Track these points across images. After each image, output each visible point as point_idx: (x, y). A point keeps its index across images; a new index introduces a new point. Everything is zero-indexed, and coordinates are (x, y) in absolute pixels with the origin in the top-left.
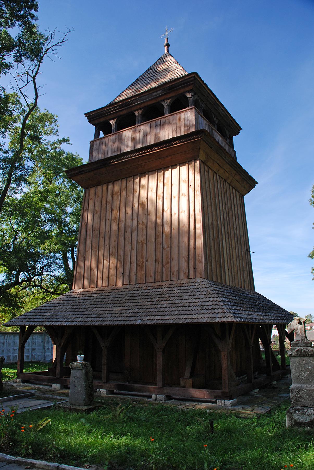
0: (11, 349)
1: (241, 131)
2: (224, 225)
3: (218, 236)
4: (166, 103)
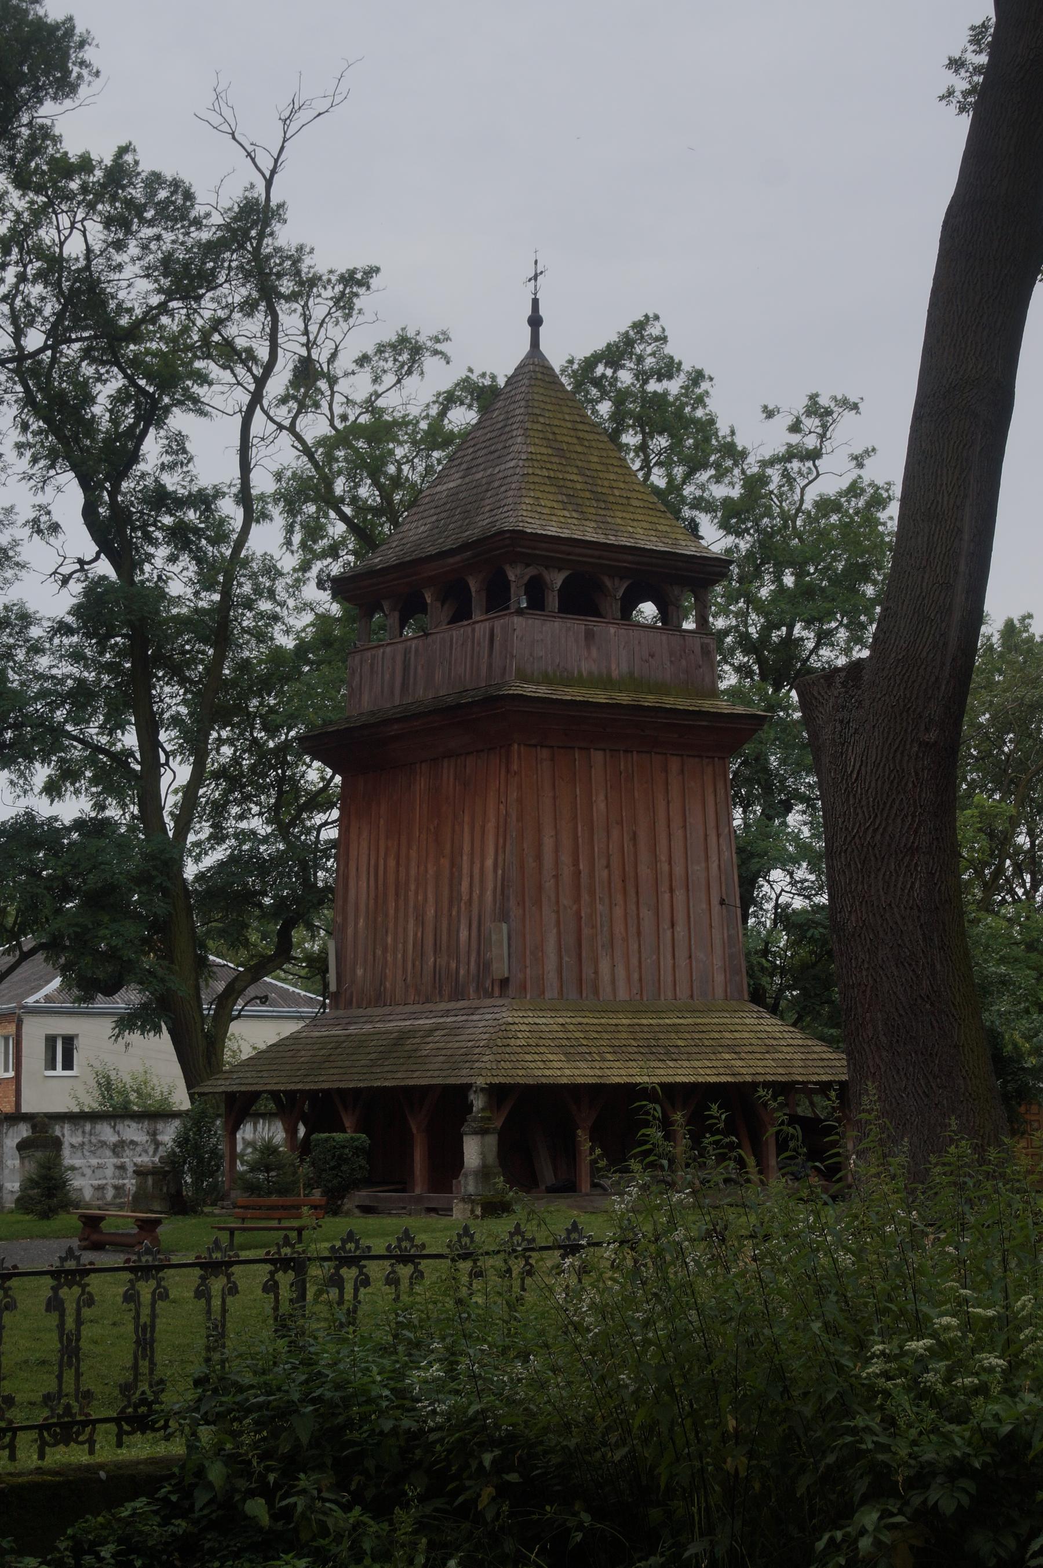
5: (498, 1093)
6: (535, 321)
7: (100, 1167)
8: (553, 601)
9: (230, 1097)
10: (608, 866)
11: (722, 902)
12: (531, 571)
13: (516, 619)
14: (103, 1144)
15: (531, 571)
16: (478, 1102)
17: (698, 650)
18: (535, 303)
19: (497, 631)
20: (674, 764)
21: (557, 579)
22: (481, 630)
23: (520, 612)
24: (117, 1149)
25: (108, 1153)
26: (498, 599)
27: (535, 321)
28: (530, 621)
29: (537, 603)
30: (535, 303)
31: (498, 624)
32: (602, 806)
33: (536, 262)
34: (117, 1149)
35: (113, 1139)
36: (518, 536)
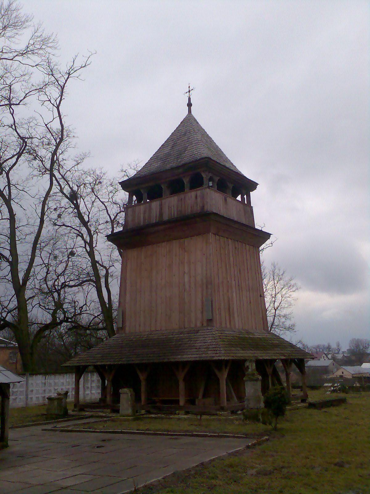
0: (52, 388)
1: (258, 186)
2: (235, 280)
3: (228, 291)
4: (186, 181)
6: (190, 105)
12: (210, 175)
15: (210, 175)
18: (189, 99)
23: (209, 187)
27: (190, 105)
28: (211, 191)
30: (189, 99)
33: (189, 87)
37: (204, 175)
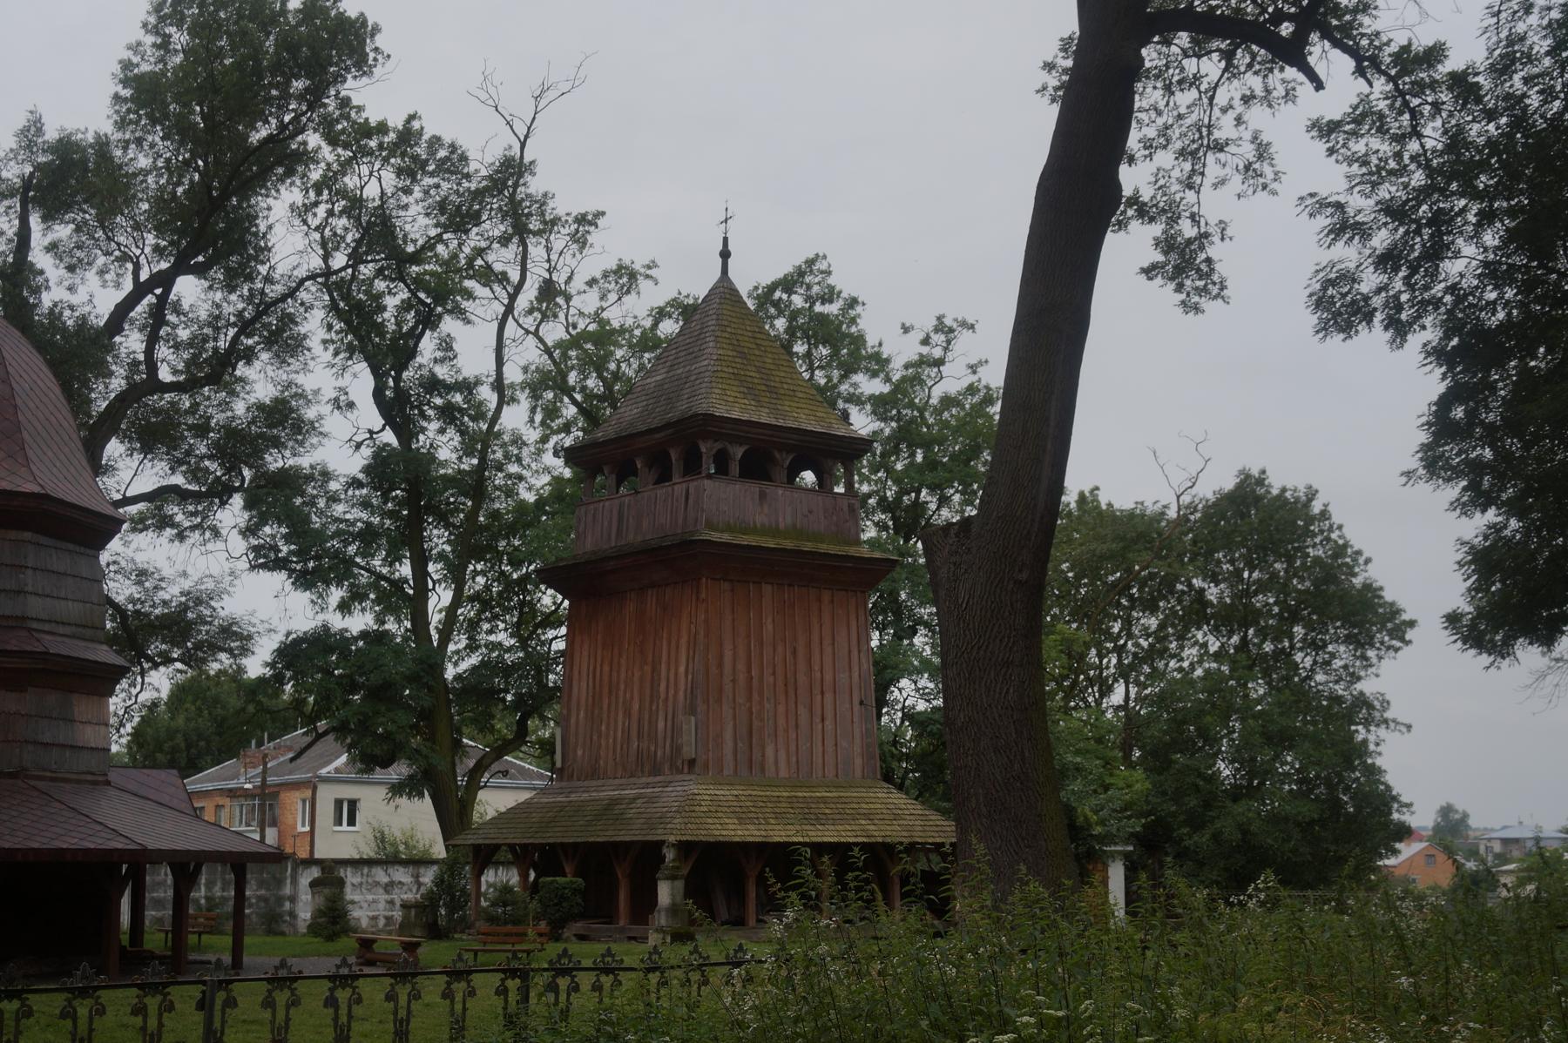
5: (685, 848)
6: (725, 254)
7: (374, 901)
8: (735, 469)
9: (477, 849)
10: (774, 673)
11: (861, 703)
12: (718, 446)
13: (706, 482)
14: (377, 884)
15: (718, 446)
16: (670, 855)
17: (846, 508)
18: (726, 240)
19: (692, 491)
20: (826, 596)
21: (738, 452)
22: (679, 489)
23: (709, 476)
24: (389, 887)
25: (381, 891)
26: (692, 466)
27: (725, 254)
29: (722, 470)
30: (726, 240)
31: (692, 485)
32: (770, 627)
34: (389, 887)
35: (385, 880)
36: (710, 418)
37: (703, 450)
